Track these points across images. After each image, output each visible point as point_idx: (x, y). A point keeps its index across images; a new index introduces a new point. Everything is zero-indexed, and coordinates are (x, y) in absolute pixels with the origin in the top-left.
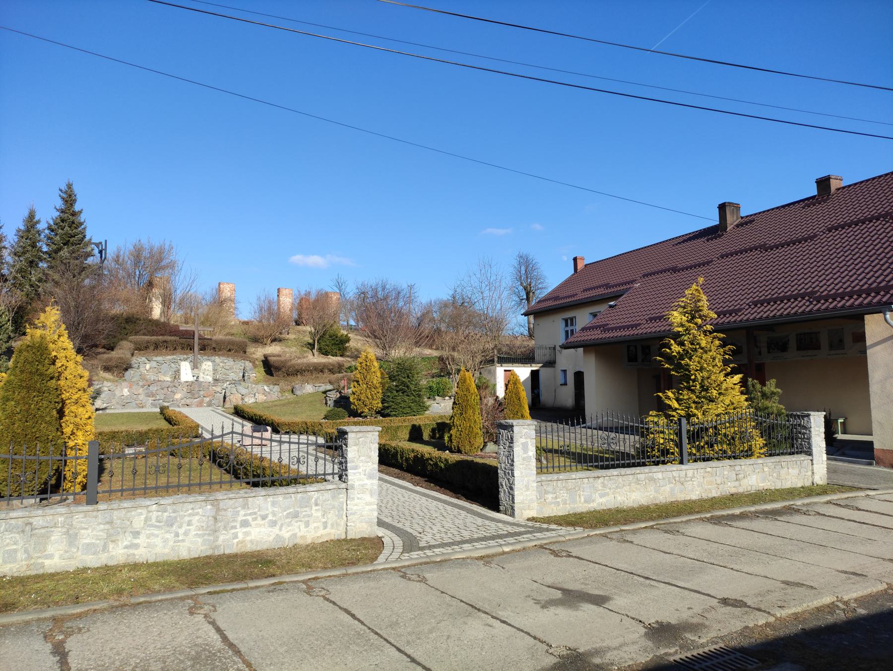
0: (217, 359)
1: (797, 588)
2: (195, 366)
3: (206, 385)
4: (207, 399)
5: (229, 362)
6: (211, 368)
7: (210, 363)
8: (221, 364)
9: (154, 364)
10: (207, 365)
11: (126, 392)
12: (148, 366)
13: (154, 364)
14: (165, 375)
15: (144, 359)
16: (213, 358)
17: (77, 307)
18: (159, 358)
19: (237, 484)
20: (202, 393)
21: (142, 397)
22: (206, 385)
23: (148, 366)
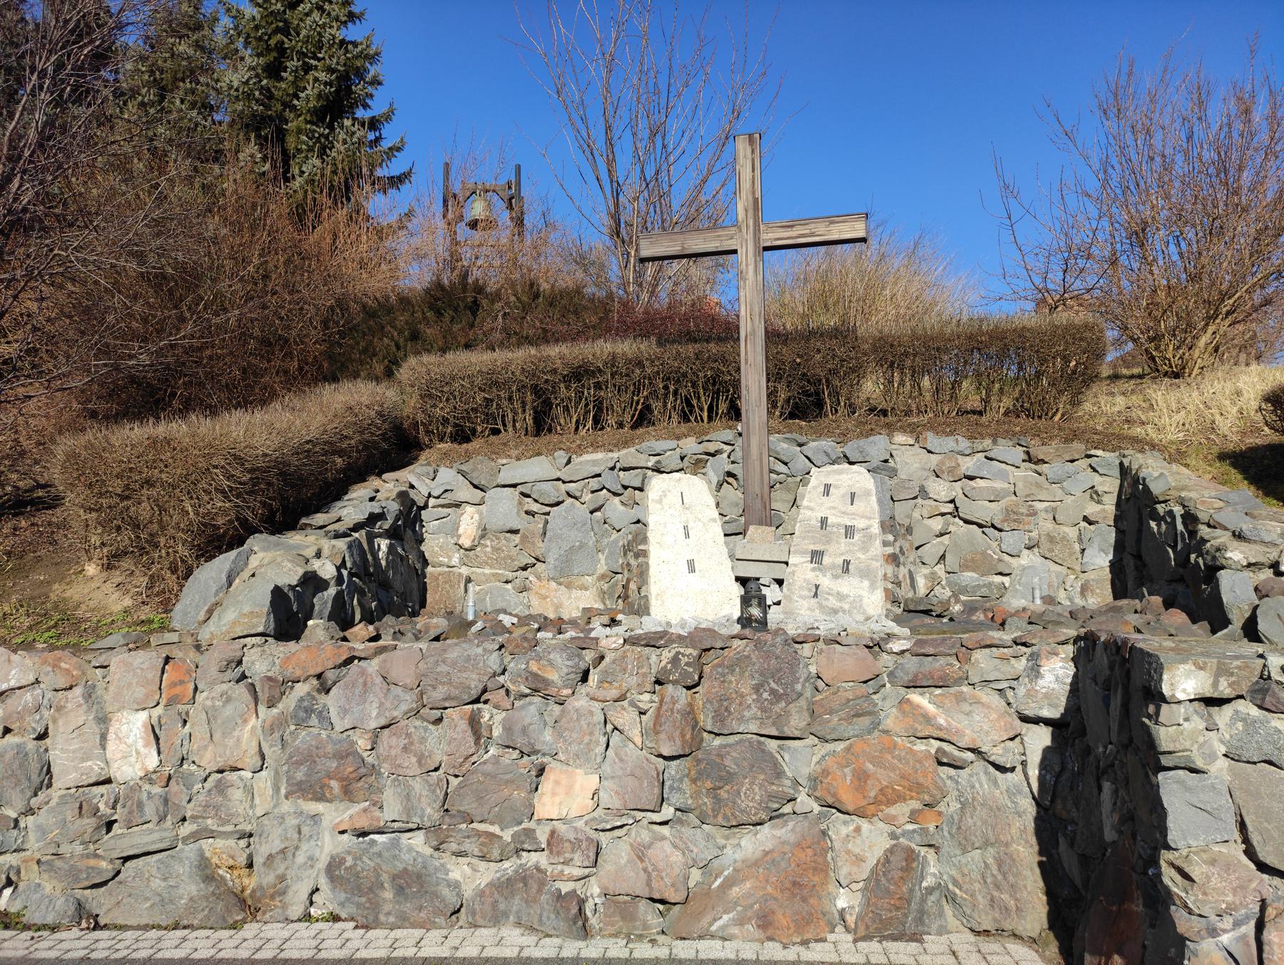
0: (909, 457)
1: (1250, 828)
2: (755, 509)
3: (844, 665)
4: (863, 842)
5: (1001, 473)
6: (868, 515)
7: (859, 478)
8: (941, 490)
9: (504, 507)
10: (839, 493)
11: (130, 751)
12: (468, 522)
13: (504, 507)
14: (565, 577)
15: (447, 475)
16: (877, 446)
17: (355, 326)
18: (535, 468)
19: (710, 625)
20: (801, 760)
21: (258, 796)
22: (844, 665)
23: (468, 522)
